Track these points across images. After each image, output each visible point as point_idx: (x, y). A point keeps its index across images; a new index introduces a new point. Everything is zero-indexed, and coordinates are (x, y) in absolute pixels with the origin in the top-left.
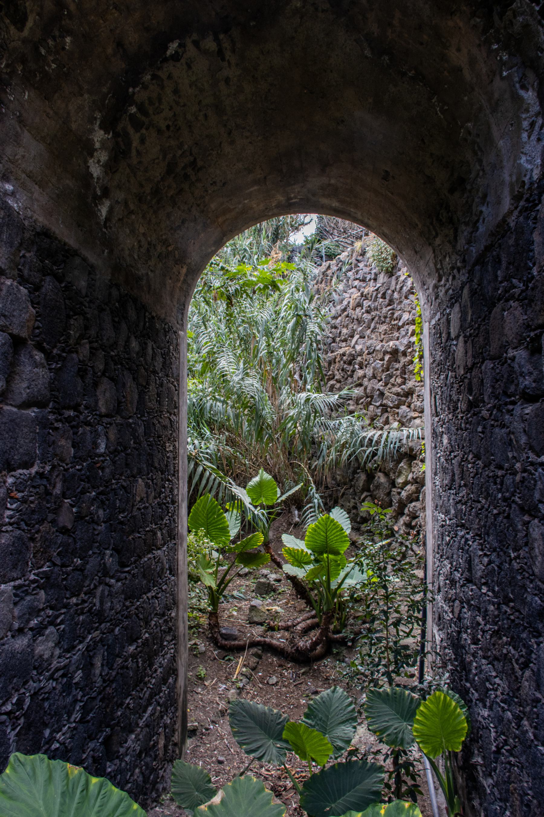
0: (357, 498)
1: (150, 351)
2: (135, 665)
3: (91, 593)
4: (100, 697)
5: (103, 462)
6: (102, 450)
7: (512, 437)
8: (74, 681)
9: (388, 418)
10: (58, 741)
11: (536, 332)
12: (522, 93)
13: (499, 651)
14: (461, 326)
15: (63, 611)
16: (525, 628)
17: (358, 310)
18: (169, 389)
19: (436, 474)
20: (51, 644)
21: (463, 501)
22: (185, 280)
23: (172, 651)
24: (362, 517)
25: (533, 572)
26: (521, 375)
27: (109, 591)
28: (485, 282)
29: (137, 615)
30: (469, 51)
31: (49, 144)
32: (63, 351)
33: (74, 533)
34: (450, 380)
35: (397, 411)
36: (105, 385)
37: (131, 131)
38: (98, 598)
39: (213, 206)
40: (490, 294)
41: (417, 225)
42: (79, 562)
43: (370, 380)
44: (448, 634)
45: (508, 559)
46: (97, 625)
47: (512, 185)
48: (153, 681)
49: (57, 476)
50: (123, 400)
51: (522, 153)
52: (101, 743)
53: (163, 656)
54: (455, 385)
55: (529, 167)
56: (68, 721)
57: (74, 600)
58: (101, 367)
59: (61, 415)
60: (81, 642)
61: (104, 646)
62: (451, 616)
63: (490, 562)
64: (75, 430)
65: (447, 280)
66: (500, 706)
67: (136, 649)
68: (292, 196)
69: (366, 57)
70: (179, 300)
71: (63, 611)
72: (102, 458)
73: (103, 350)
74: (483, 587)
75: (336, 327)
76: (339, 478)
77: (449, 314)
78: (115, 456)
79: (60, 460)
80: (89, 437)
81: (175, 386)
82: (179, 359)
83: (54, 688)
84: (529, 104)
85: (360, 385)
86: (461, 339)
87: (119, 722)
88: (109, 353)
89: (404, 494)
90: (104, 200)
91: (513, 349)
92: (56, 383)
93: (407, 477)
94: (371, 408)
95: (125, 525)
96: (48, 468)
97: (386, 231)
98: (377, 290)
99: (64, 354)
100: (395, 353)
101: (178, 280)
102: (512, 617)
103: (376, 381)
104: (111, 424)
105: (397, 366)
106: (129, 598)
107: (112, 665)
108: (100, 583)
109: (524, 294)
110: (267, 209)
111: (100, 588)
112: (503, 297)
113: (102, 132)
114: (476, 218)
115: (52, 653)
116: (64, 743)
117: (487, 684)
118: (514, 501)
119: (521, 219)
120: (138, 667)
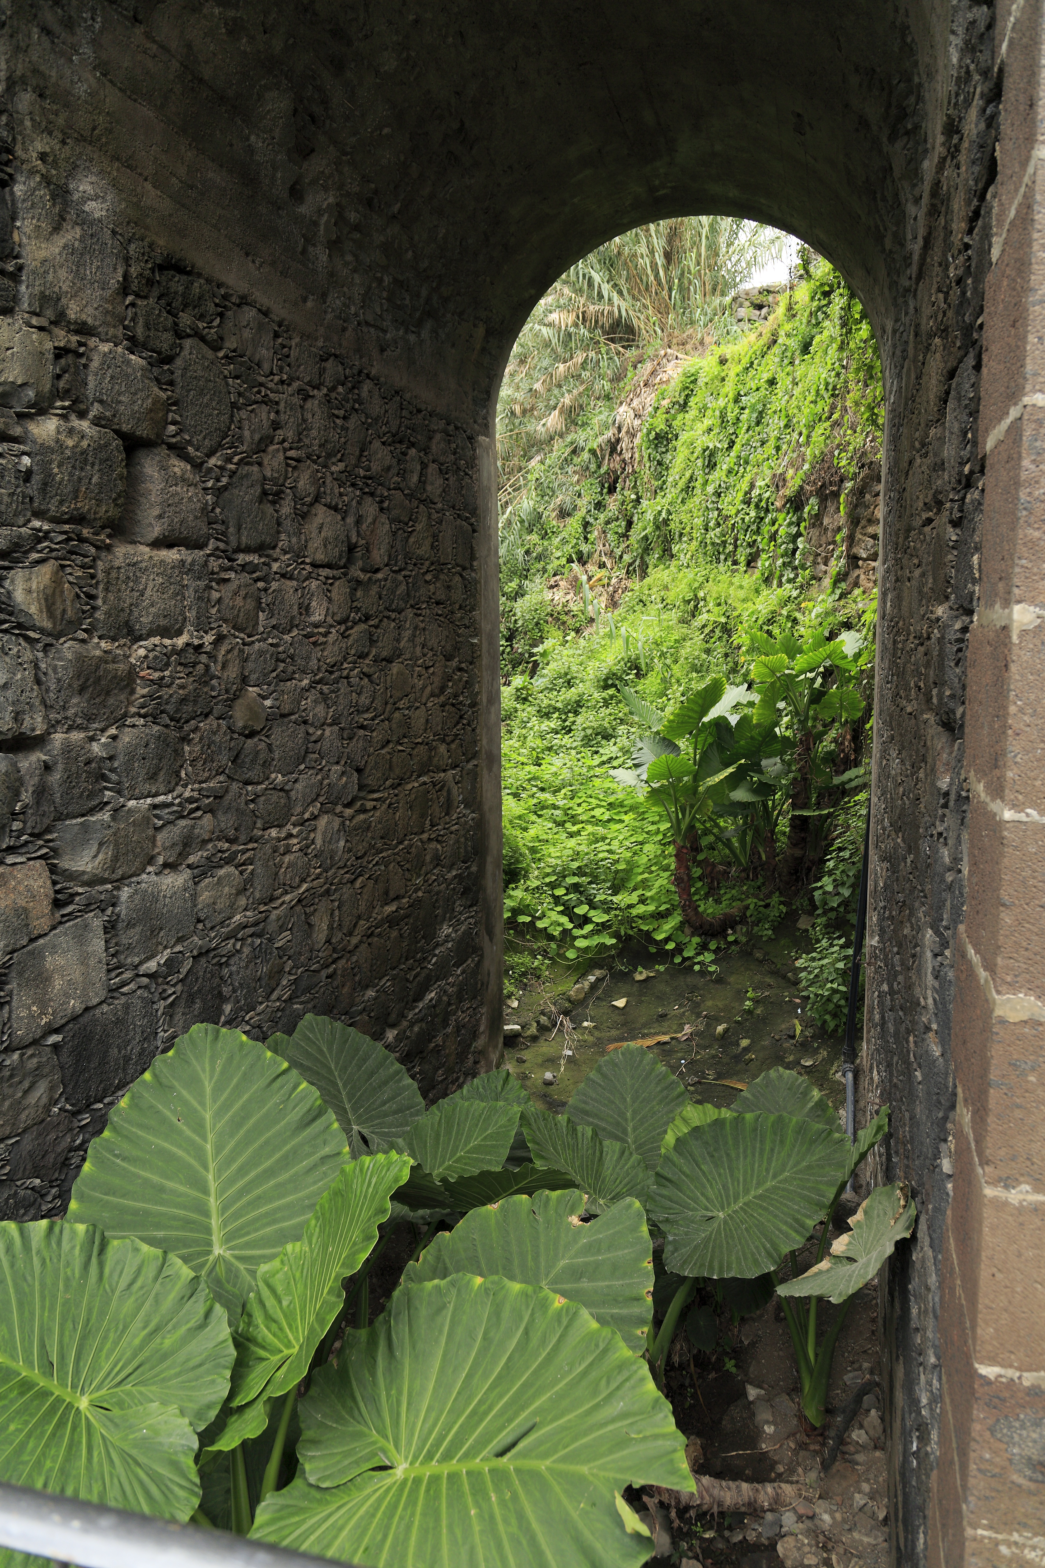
5: (326, 635)
22: (483, 349)
36: (321, 514)
68: (657, 182)
72: (322, 630)
96: (209, 638)
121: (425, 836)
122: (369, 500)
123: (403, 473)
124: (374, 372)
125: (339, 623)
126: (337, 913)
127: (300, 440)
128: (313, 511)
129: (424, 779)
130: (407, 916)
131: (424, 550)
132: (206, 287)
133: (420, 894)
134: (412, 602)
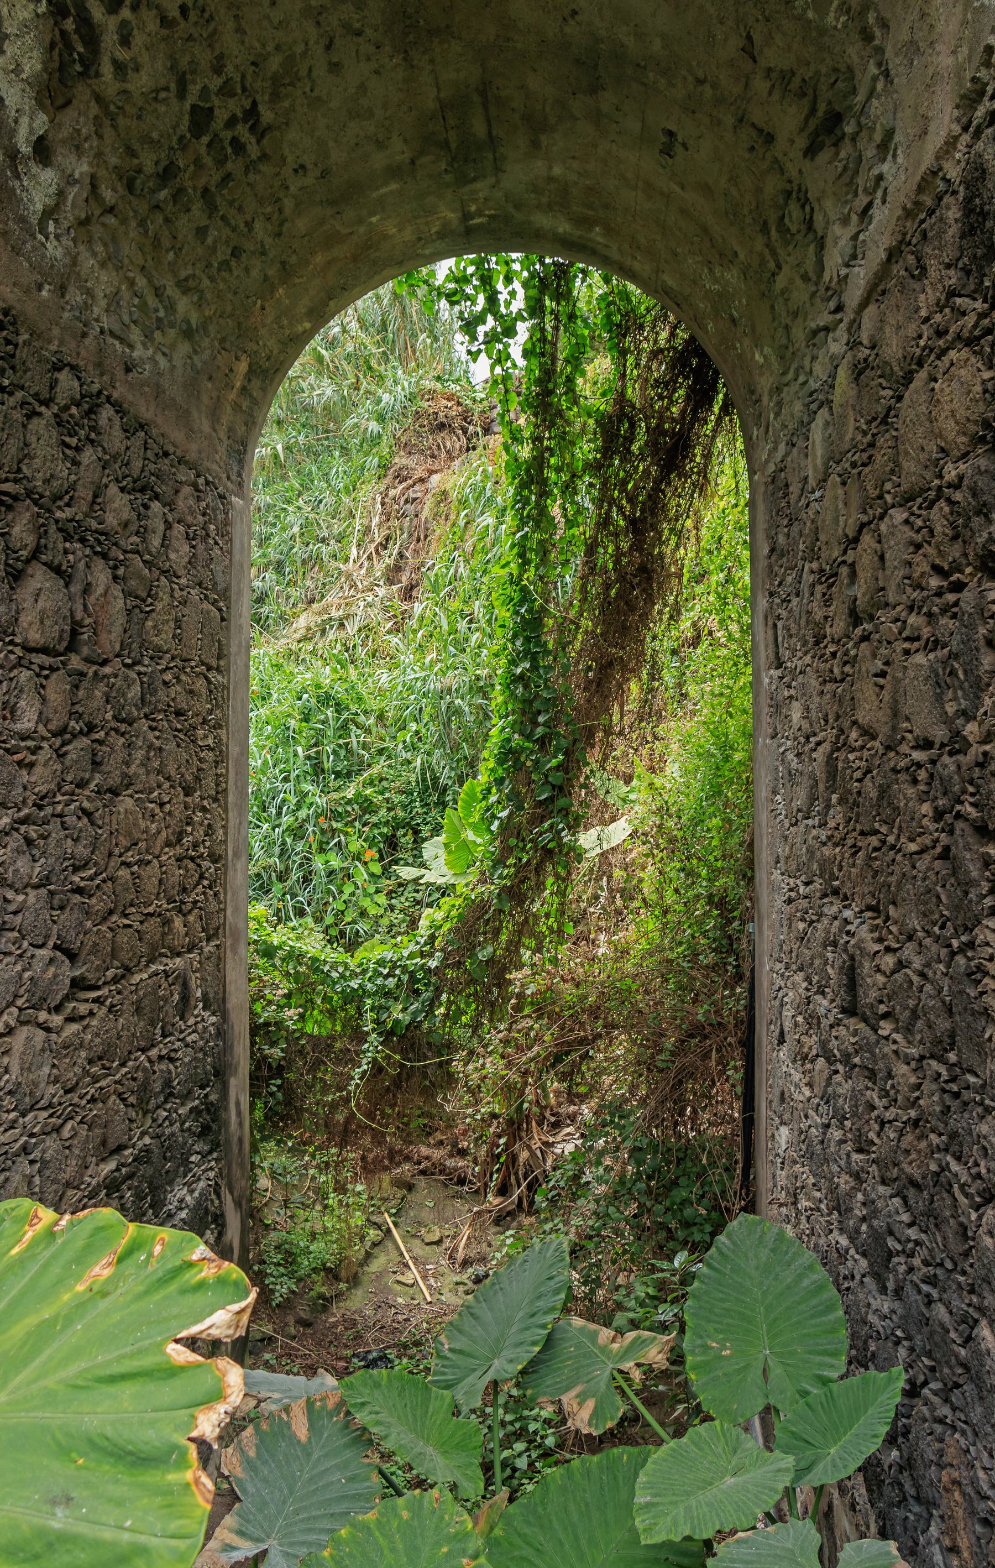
5: (34, 751)
13: (919, 1167)
22: (244, 388)
23: (211, 1174)
34: (808, 578)
36: (39, 578)
45: (944, 952)
46: (13, 1115)
58: (30, 540)
62: (808, 1094)
63: (901, 965)
67: (117, 1170)
68: (473, 208)
70: (230, 429)
72: (31, 743)
74: (882, 1023)
81: (220, 610)
82: (230, 552)
104: (53, 669)
106: (100, 1058)
110: (420, 239)
118: (959, 816)
121: (154, 1052)
122: (99, 563)
123: (143, 533)
124: (115, 395)
125: (54, 735)
126: (37, 1180)
127: (19, 470)
128: (30, 571)
129: (153, 968)
130: (130, 1176)
131: (164, 639)
133: (147, 1140)
134: (146, 710)
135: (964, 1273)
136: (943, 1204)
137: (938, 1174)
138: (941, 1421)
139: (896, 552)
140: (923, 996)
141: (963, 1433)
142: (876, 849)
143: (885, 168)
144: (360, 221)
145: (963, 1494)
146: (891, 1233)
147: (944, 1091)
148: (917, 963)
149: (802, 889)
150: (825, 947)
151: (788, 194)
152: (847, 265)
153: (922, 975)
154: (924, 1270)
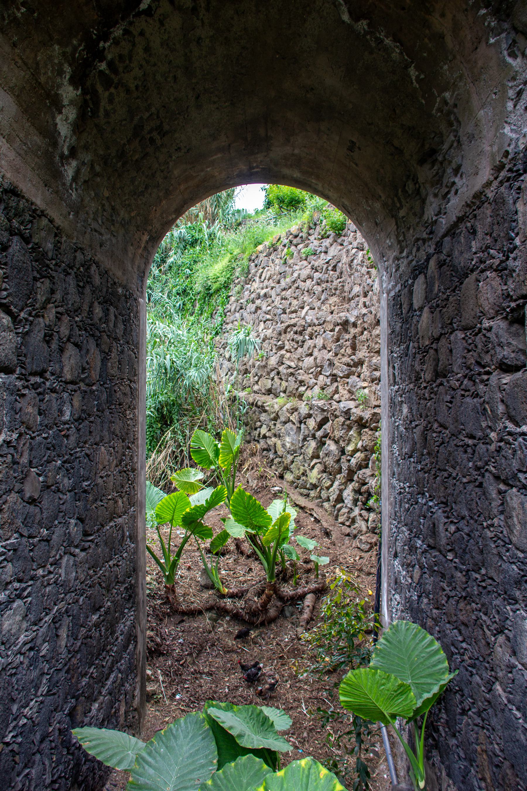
0: (306, 465)
1: (112, 318)
2: (98, 634)
3: (56, 563)
4: (66, 668)
5: (68, 429)
6: (67, 418)
7: (487, 406)
8: (41, 654)
9: (337, 387)
10: (25, 716)
11: (517, 303)
12: (509, 60)
14: (426, 298)
15: (31, 583)
16: (499, 595)
17: (309, 282)
18: (130, 356)
19: (393, 442)
20: (18, 618)
21: (426, 469)
22: (145, 247)
23: (132, 618)
24: (311, 484)
25: (510, 540)
26: (499, 345)
27: (75, 561)
28: (456, 252)
29: (100, 584)
30: (454, 16)
31: (18, 96)
32: (30, 315)
33: (40, 503)
34: (411, 351)
35: (347, 380)
36: (71, 350)
37: (100, 89)
38: (63, 568)
39: (176, 172)
40: (462, 264)
41: (380, 197)
42: (46, 532)
43: (320, 350)
44: (406, 598)
47: (493, 156)
48: (115, 649)
49: (24, 444)
50: (88, 366)
51: (506, 122)
52: (67, 715)
53: (124, 623)
54: (417, 355)
55: (514, 136)
56: (36, 695)
57: (41, 572)
58: (67, 332)
59: (28, 381)
60: (47, 614)
61: (69, 616)
62: (410, 581)
63: (458, 530)
64: (41, 397)
65: (410, 253)
66: (467, 670)
69: (343, 22)
70: (139, 267)
71: (31, 583)
72: (67, 426)
73: (69, 315)
75: (286, 299)
76: (288, 445)
77: (412, 285)
78: (80, 424)
79: (27, 428)
80: (55, 405)
82: (139, 326)
83: (22, 663)
84: (517, 72)
85: (311, 355)
86: (426, 309)
87: (83, 692)
88: (73, 318)
89: (353, 461)
90: (70, 160)
91: (489, 319)
92: (23, 347)
93: (356, 445)
94: (321, 377)
95: (89, 493)
96: (15, 436)
97: (346, 203)
98: (327, 263)
99: (31, 318)
100: (345, 324)
101: (139, 247)
102: (484, 584)
103: (326, 351)
105: (347, 336)
107: (77, 636)
108: (65, 553)
109: (504, 264)
111: (66, 558)
112: (478, 268)
113: (71, 88)
114: (447, 190)
115: (20, 627)
116: (31, 718)
117: (452, 648)
118: (487, 470)
119: (502, 189)
120: (101, 636)
132: (26, 204)
135: (488, 662)
136: (478, 633)
137: (476, 620)
138: (476, 725)
139: (459, 351)
140: (469, 544)
141: (488, 730)
142: (446, 478)
143: (457, 180)
144: (202, 170)
145: (488, 755)
146: (453, 645)
147: (479, 586)
148: (466, 530)
149: (407, 490)
150: (419, 517)
151: (408, 177)
152: (436, 215)
153: (468, 535)
154: (469, 661)
